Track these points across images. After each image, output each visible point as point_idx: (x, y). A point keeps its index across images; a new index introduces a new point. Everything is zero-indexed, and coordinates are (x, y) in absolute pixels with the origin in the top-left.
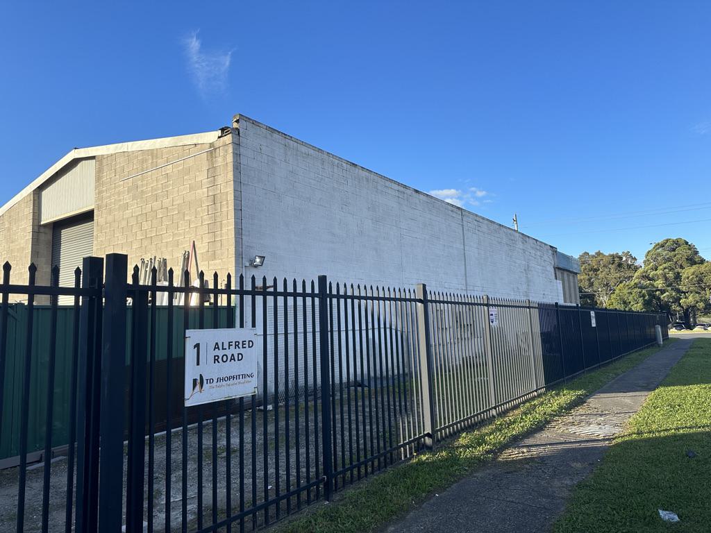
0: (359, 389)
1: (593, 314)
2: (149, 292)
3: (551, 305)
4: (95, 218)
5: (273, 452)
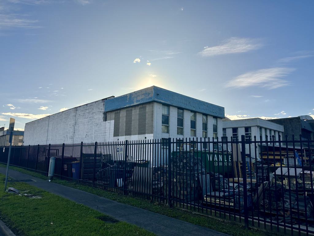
0: (234, 145)
1: (4, 148)
2: (4, 151)
3: (37, 146)
4: (241, 136)
5: (203, 179)
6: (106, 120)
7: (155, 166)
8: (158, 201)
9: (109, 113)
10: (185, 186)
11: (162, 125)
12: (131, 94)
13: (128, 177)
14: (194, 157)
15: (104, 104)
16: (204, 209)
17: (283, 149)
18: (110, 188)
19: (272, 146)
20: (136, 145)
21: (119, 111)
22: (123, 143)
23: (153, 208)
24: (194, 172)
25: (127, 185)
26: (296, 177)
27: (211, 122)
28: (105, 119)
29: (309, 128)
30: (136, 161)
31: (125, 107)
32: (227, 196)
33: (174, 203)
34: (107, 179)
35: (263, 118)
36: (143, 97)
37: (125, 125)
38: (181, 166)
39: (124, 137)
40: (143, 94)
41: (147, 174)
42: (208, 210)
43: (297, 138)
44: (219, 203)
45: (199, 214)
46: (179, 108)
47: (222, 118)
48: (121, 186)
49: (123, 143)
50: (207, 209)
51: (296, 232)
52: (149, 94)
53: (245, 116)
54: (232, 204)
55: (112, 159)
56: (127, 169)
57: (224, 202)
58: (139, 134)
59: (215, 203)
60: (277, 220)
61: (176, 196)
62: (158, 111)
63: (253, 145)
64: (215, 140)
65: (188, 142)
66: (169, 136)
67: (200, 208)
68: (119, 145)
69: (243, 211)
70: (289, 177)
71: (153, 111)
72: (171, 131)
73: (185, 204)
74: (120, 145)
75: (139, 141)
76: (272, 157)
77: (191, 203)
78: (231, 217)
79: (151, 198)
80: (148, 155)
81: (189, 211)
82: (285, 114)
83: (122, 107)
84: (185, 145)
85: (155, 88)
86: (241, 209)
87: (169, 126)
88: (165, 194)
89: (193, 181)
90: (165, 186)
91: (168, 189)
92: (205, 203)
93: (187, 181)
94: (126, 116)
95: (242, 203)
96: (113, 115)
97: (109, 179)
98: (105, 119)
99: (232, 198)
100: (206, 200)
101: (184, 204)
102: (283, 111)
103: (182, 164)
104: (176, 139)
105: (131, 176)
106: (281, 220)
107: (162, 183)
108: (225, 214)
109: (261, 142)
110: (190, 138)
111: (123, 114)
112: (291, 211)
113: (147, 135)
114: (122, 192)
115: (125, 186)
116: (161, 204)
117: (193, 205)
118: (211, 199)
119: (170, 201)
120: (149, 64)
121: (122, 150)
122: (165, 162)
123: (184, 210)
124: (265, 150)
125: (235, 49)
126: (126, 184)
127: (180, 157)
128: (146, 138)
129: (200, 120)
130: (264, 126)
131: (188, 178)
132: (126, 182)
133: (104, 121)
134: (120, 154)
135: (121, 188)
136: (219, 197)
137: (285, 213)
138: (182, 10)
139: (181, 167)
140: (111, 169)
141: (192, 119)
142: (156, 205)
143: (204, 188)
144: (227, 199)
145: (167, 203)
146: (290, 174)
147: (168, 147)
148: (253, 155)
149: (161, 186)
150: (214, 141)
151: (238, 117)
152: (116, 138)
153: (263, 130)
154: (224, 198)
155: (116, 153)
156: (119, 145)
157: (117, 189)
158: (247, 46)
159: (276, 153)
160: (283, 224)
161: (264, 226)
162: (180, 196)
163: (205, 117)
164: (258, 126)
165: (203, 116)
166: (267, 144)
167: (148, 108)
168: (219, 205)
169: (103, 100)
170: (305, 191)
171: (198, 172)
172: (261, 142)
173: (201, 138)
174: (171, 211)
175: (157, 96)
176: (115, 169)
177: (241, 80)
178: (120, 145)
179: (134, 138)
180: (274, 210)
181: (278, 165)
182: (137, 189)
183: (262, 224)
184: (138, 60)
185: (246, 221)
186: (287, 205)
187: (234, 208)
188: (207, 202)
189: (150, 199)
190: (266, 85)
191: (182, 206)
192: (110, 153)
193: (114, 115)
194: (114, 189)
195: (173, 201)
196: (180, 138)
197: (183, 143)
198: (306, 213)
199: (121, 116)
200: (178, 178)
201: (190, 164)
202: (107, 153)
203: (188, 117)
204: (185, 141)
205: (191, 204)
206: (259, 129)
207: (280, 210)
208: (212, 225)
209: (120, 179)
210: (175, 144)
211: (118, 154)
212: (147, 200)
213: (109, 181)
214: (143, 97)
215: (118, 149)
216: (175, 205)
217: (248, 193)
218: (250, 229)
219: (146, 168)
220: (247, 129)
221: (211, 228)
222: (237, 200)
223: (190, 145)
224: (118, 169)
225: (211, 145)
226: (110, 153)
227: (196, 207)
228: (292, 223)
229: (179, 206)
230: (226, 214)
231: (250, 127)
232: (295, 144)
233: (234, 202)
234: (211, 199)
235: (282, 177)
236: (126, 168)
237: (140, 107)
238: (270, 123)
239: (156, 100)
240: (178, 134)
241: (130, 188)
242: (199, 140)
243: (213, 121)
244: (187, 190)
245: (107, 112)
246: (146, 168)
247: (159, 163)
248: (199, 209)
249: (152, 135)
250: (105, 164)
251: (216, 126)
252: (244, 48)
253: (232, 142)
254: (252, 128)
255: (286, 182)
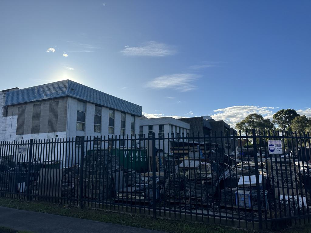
0: (161, 141)
6: (6, 116)
7: (66, 166)
8: (68, 203)
9: (12, 108)
10: (98, 185)
11: (77, 122)
12: (40, 87)
13: (32, 181)
14: (108, 155)
15: (4, 97)
16: (116, 205)
17: (191, 144)
18: (9, 195)
19: (177, 141)
20: (46, 144)
21: (24, 106)
22: (27, 143)
23: (62, 211)
24: (108, 170)
25: (31, 190)
26: (195, 168)
27: (129, 120)
28: (6, 114)
29: (209, 126)
30: (43, 161)
31: (32, 101)
32: (138, 191)
33: (85, 203)
34: (5, 185)
35: (175, 117)
36: (55, 90)
37: (31, 121)
38: (95, 164)
39: (46, 134)
40: (55, 88)
41: (56, 175)
42: (120, 206)
43: (201, 135)
44: (130, 198)
45: (111, 211)
46: (97, 105)
47: (139, 116)
48: (24, 191)
49: (27, 143)
50: (136, 207)
51: (194, 216)
52: (62, 88)
53: (160, 115)
54: (143, 198)
55: (14, 161)
56: (31, 172)
57: (136, 197)
58: (49, 132)
59: (127, 199)
60: (180, 207)
61: (88, 196)
62: (73, 108)
63: (166, 141)
64: (134, 138)
65: (106, 140)
66: (85, 133)
67: (112, 205)
68: (22, 145)
69: (152, 203)
70: (190, 168)
71: (66, 107)
72: (87, 129)
73: (97, 203)
74: (21, 144)
75: (53, 139)
76: (182, 152)
77: (103, 201)
78: (141, 210)
79: (60, 201)
80: (60, 155)
81: (101, 210)
82: (192, 114)
83: (28, 101)
84: (103, 143)
85: (69, 82)
86: (150, 201)
87: (85, 123)
88: (76, 195)
89: (106, 179)
90: (76, 187)
91: (79, 189)
92: (117, 200)
93: (100, 180)
94: (34, 111)
95: (151, 195)
96: (16, 110)
97: (8, 185)
98: (6, 114)
99: (142, 192)
100: (119, 196)
101: (96, 203)
102: (191, 112)
103: (95, 163)
104: (94, 136)
105: (36, 180)
106: (184, 208)
107: (73, 184)
108: (136, 208)
109: (173, 138)
110: (109, 136)
111: (29, 109)
112: (191, 198)
113: (58, 133)
114: (25, 198)
115: (29, 191)
116: (71, 206)
117: (105, 203)
118: (123, 195)
119: (82, 202)
120: (66, 55)
121: (25, 151)
122: (77, 162)
123: (95, 210)
124: (175, 145)
125: (153, 53)
126: (30, 189)
127: (93, 156)
128: (57, 136)
129: (118, 117)
130: (174, 124)
131: (102, 176)
132: (30, 187)
133: (4, 116)
134: (23, 154)
135: (23, 193)
136: (131, 193)
137: (186, 200)
138: (104, 5)
139: (94, 165)
140: (11, 173)
141: (110, 117)
142: (65, 208)
143: (117, 185)
144: (138, 193)
145: (77, 205)
146: (191, 166)
147: (80, 146)
148: (166, 151)
149: (71, 187)
150: (133, 138)
151: (154, 115)
152: (20, 137)
153: (174, 128)
154: (136, 192)
155: (18, 154)
156: (22, 145)
157: (18, 195)
158: (164, 51)
159: (185, 148)
160: (184, 210)
161: (169, 215)
162: (92, 196)
163: (123, 115)
164: (170, 124)
165: (122, 114)
166: (173, 140)
167: (61, 103)
168: (130, 200)
169: (3, 91)
170: (201, 180)
171: (111, 170)
172: (173, 138)
173: (120, 136)
174: (82, 212)
175: (71, 91)
176: (15, 173)
177: (159, 82)
178: (23, 144)
179: (43, 136)
180: (178, 199)
181: (186, 158)
182: (43, 193)
183: (167, 213)
184: (53, 50)
185: (155, 212)
186: (188, 194)
187: (144, 201)
188: (119, 198)
189: (59, 202)
190: (179, 88)
191: (94, 206)
192: (12, 154)
193: (18, 110)
194: (14, 195)
195: (84, 201)
196: (98, 136)
197: (101, 141)
198: (202, 199)
199: (26, 111)
200: (90, 178)
201: (104, 162)
202: (6, 153)
203: (106, 115)
204: (103, 139)
205: (103, 203)
206: (170, 127)
207: (182, 199)
208: (123, 220)
209: (22, 184)
210: (92, 143)
211: (20, 154)
212: (55, 204)
213: (7, 186)
214: (55, 90)
215: (20, 149)
216: (87, 205)
217: (157, 186)
218: (158, 219)
219: (58, 170)
220: (161, 127)
221: (121, 224)
222: (147, 193)
223: (108, 142)
224: (20, 173)
225: (118, 142)
226: (12, 154)
227: (108, 205)
228: (191, 209)
229: (90, 206)
230: (137, 208)
231: (164, 125)
232: (200, 139)
233: (145, 196)
234: (123, 195)
235: (184, 169)
236: (31, 171)
237: (50, 101)
238: (179, 121)
239: (70, 95)
240: (95, 131)
241: (35, 192)
242: (118, 138)
243: (131, 119)
244: (100, 188)
245: (8, 106)
246: (58, 170)
247: (74, 163)
248: (111, 206)
249: (65, 133)
250: (307, 150)
251: (134, 124)
252: (161, 52)
253: (149, 139)
254: (165, 126)
255: (187, 173)
